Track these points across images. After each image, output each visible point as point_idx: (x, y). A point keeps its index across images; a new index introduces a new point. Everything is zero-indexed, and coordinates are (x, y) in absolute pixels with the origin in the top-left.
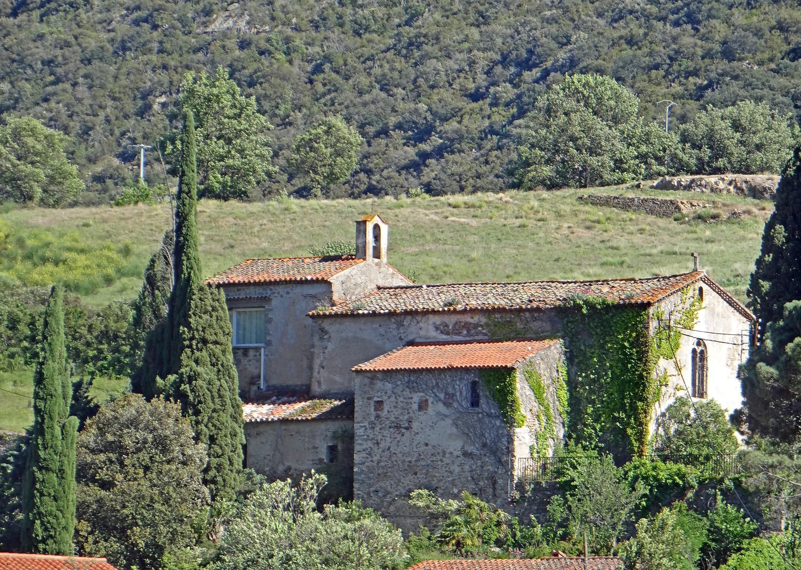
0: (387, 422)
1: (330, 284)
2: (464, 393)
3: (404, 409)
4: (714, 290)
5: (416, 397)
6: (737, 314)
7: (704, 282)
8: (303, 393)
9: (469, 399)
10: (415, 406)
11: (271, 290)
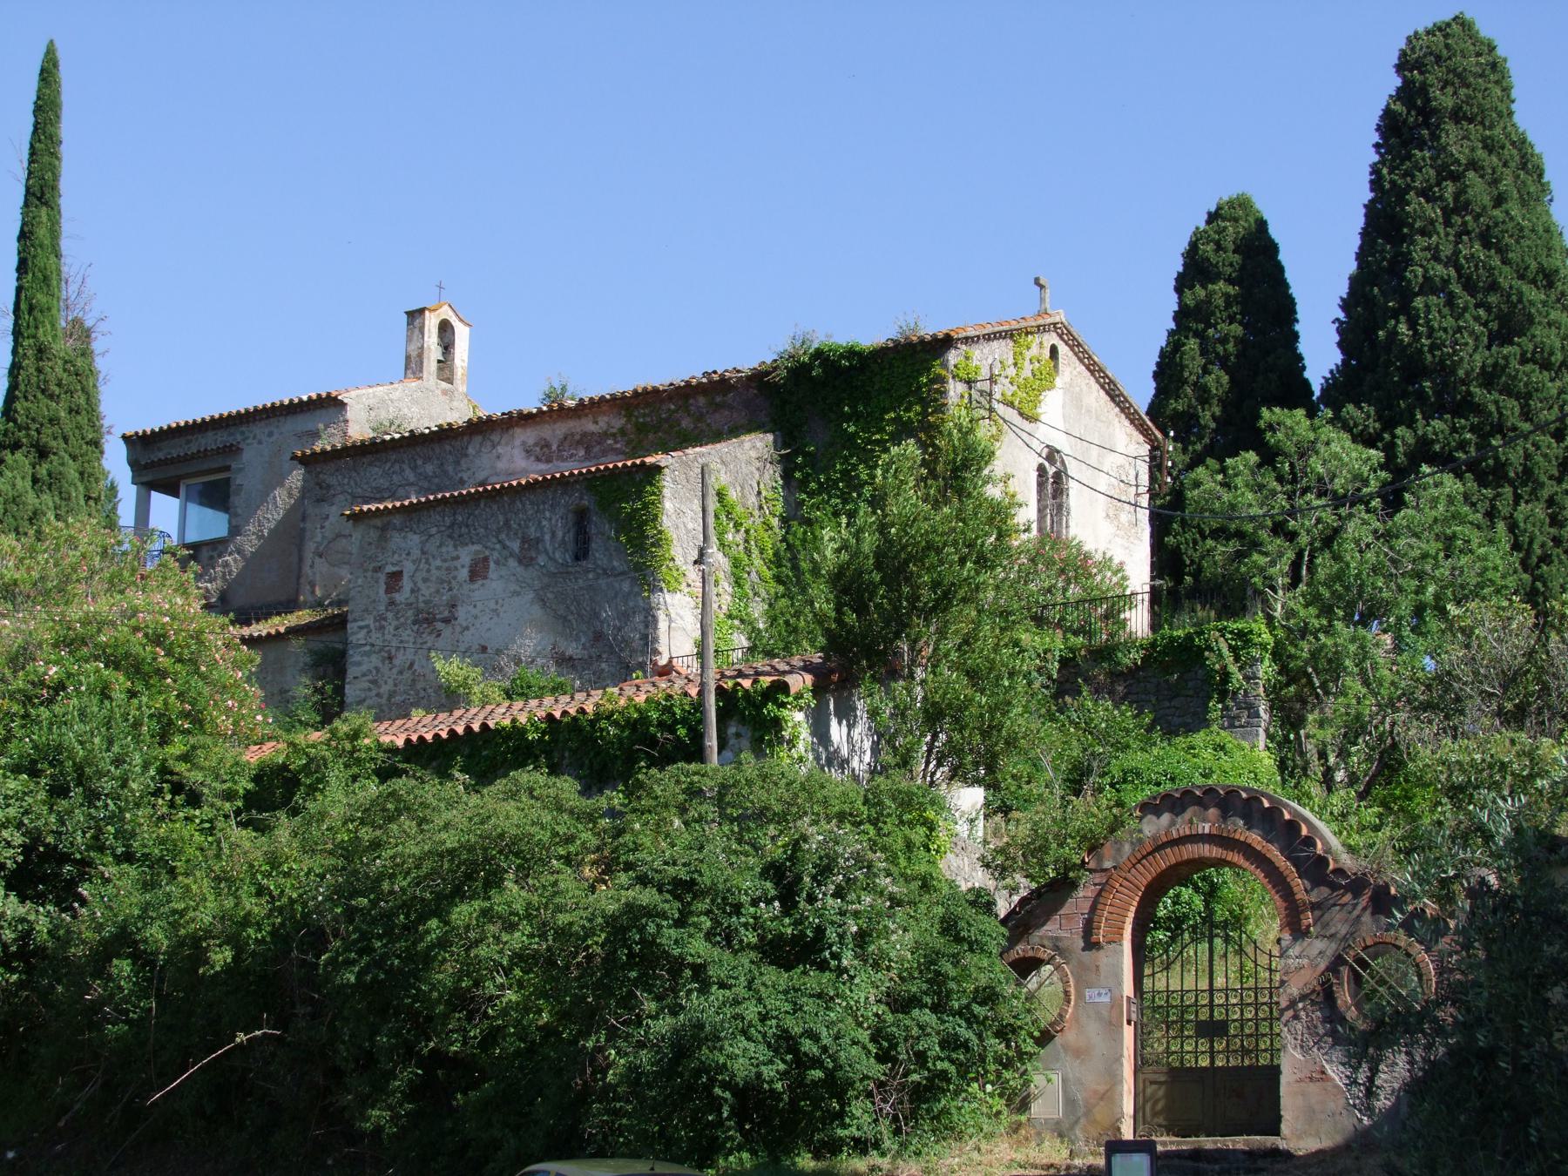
0: (410, 613)
1: (342, 405)
2: (560, 534)
3: (442, 582)
4: (1081, 360)
5: (466, 555)
6: (1127, 423)
7: (1061, 336)
8: (290, 606)
9: (571, 546)
10: (464, 574)
11: (242, 433)
